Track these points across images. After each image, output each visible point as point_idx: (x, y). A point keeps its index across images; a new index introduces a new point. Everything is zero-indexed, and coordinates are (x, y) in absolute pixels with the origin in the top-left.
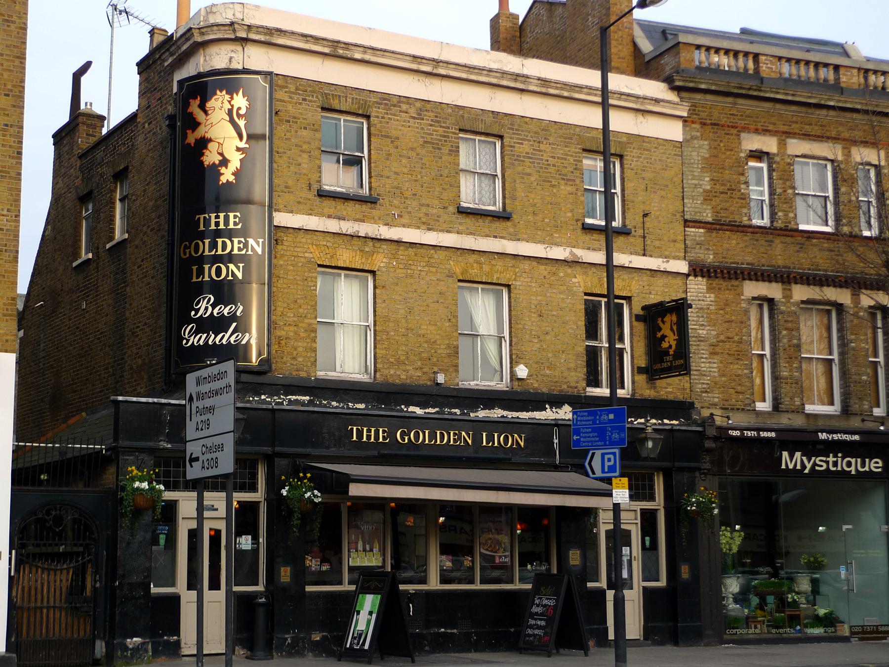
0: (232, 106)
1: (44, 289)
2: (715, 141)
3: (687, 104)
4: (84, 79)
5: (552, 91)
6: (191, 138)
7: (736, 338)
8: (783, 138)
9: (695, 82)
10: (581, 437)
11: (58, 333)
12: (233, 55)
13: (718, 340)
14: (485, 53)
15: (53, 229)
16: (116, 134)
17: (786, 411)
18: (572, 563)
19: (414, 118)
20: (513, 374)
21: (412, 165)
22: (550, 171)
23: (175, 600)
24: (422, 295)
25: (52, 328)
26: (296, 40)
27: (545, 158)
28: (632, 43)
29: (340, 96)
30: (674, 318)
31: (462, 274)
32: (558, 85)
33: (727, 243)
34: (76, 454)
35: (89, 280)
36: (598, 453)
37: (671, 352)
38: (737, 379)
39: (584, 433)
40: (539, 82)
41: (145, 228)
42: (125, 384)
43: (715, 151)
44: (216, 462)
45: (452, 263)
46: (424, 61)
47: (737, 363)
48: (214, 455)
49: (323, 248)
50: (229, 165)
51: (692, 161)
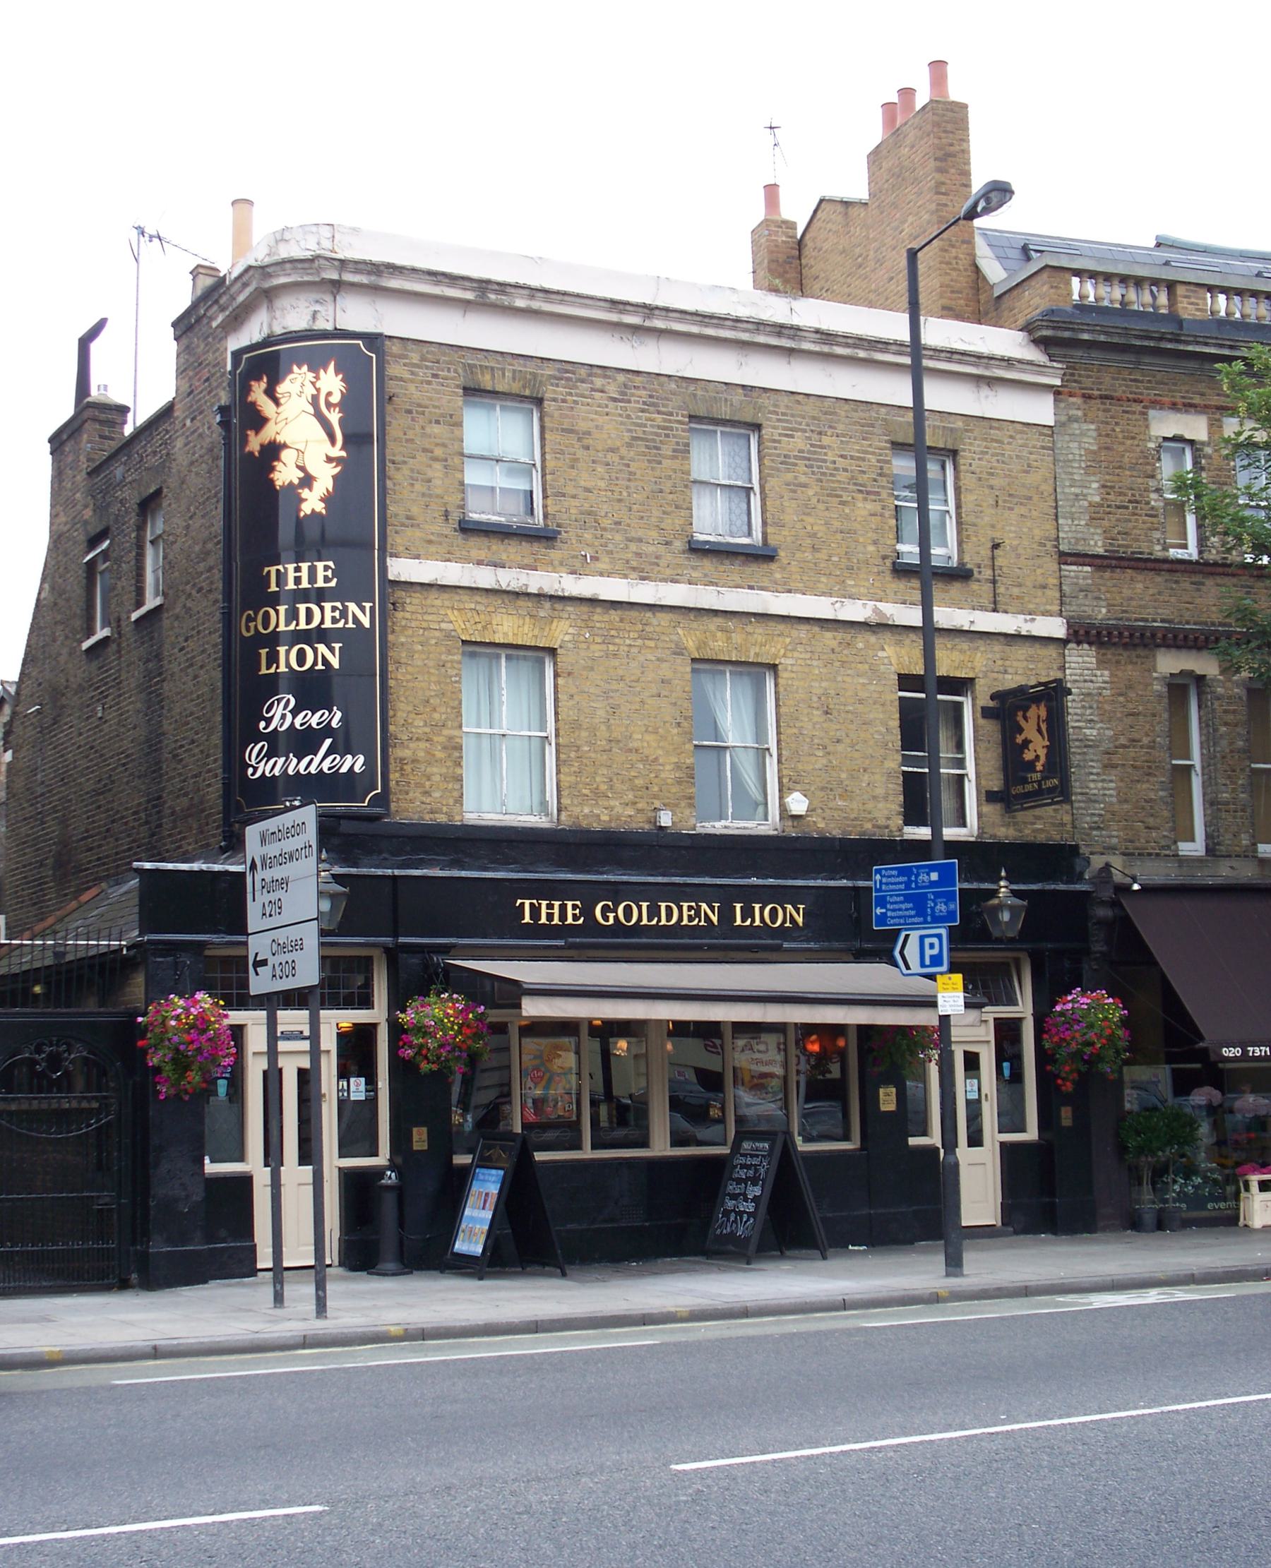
0: (318, 390)
1: (40, 684)
2: (1107, 423)
3: (1060, 366)
4: (95, 347)
5: (839, 350)
6: (255, 443)
7: (1145, 740)
8: (1217, 416)
9: (1073, 330)
10: (887, 910)
11: (62, 756)
12: (317, 307)
13: (1117, 743)
14: (728, 292)
15: (52, 588)
16: (142, 437)
17: (1228, 856)
18: (884, 1108)
19: (615, 400)
20: (783, 808)
21: (614, 475)
22: (839, 478)
23: (245, 1182)
24: (634, 684)
25: (54, 748)
26: (420, 281)
27: (830, 458)
28: (973, 268)
29: (492, 369)
30: (1043, 712)
31: (698, 649)
32: (850, 341)
33: (1129, 588)
34: (81, 955)
35: (107, 671)
36: (915, 936)
37: (1039, 767)
38: (1147, 806)
39: (892, 903)
40: (818, 336)
41: (188, 587)
42: (163, 838)
43: (1108, 440)
44: (293, 968)
45: (680, 631)
46: (628, 308)
47: (1148, 781)
48: (289, 957)
49: (470, 614)
50: (315, 484)
51: (1071, 457)
